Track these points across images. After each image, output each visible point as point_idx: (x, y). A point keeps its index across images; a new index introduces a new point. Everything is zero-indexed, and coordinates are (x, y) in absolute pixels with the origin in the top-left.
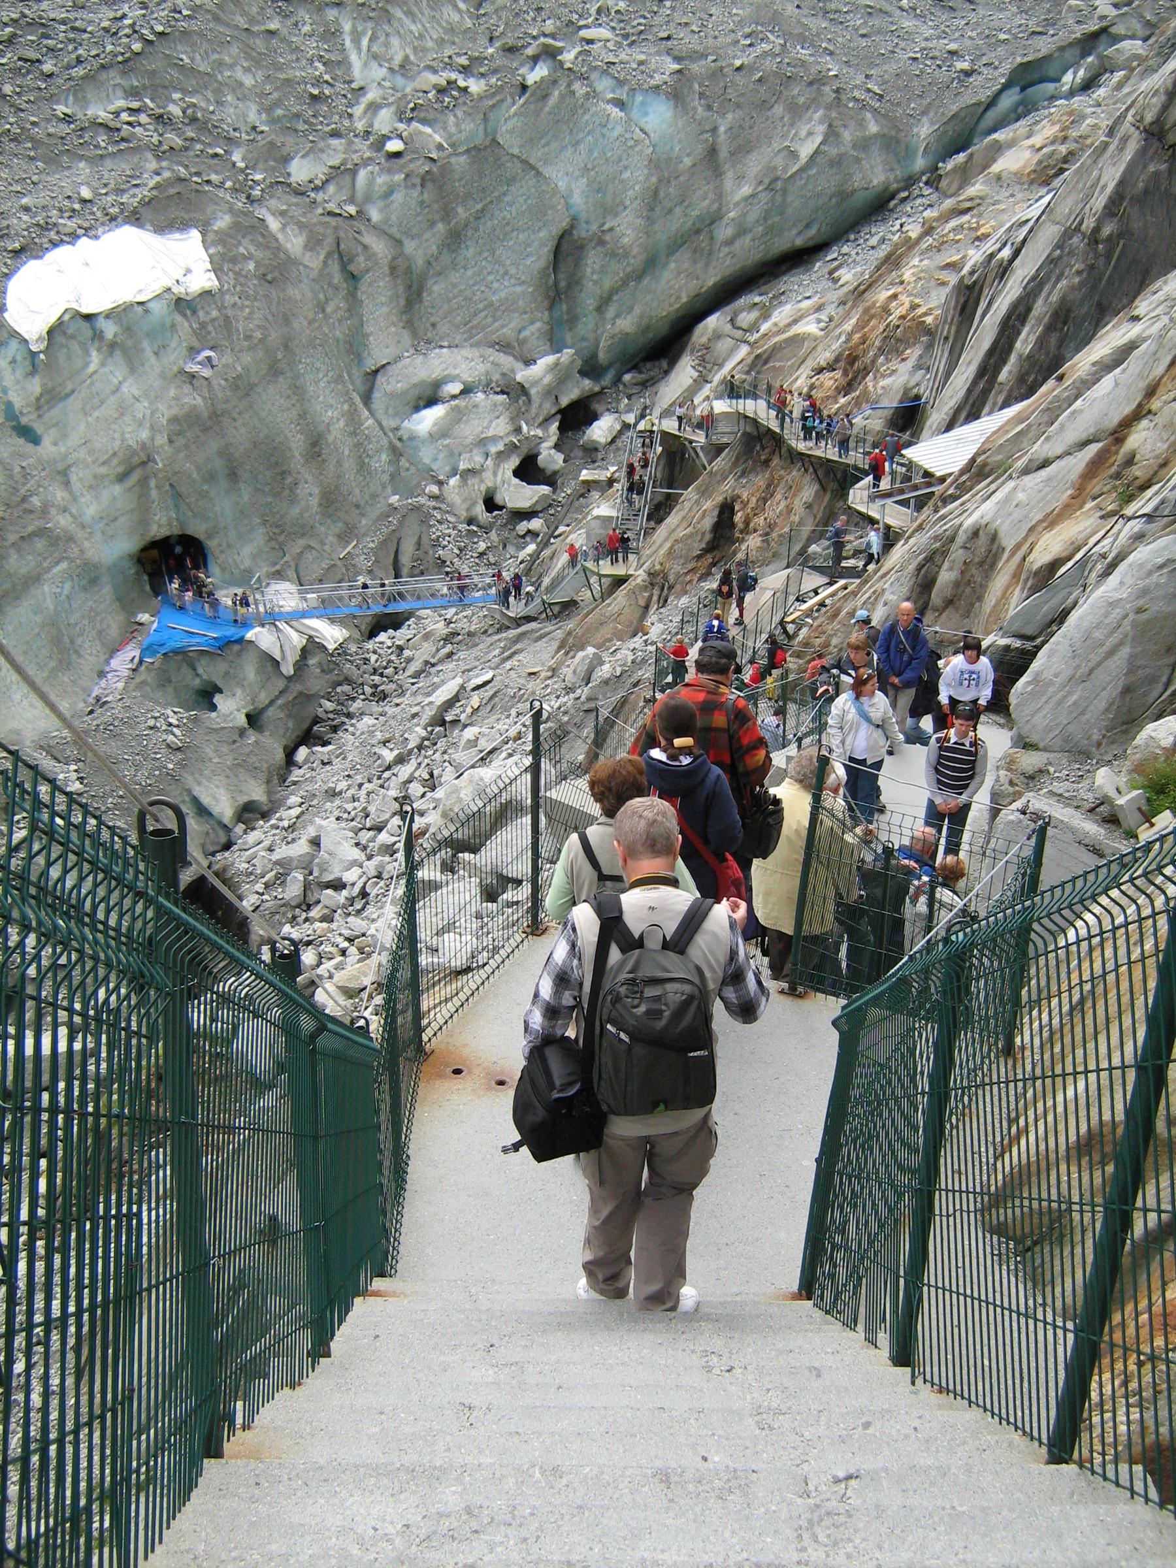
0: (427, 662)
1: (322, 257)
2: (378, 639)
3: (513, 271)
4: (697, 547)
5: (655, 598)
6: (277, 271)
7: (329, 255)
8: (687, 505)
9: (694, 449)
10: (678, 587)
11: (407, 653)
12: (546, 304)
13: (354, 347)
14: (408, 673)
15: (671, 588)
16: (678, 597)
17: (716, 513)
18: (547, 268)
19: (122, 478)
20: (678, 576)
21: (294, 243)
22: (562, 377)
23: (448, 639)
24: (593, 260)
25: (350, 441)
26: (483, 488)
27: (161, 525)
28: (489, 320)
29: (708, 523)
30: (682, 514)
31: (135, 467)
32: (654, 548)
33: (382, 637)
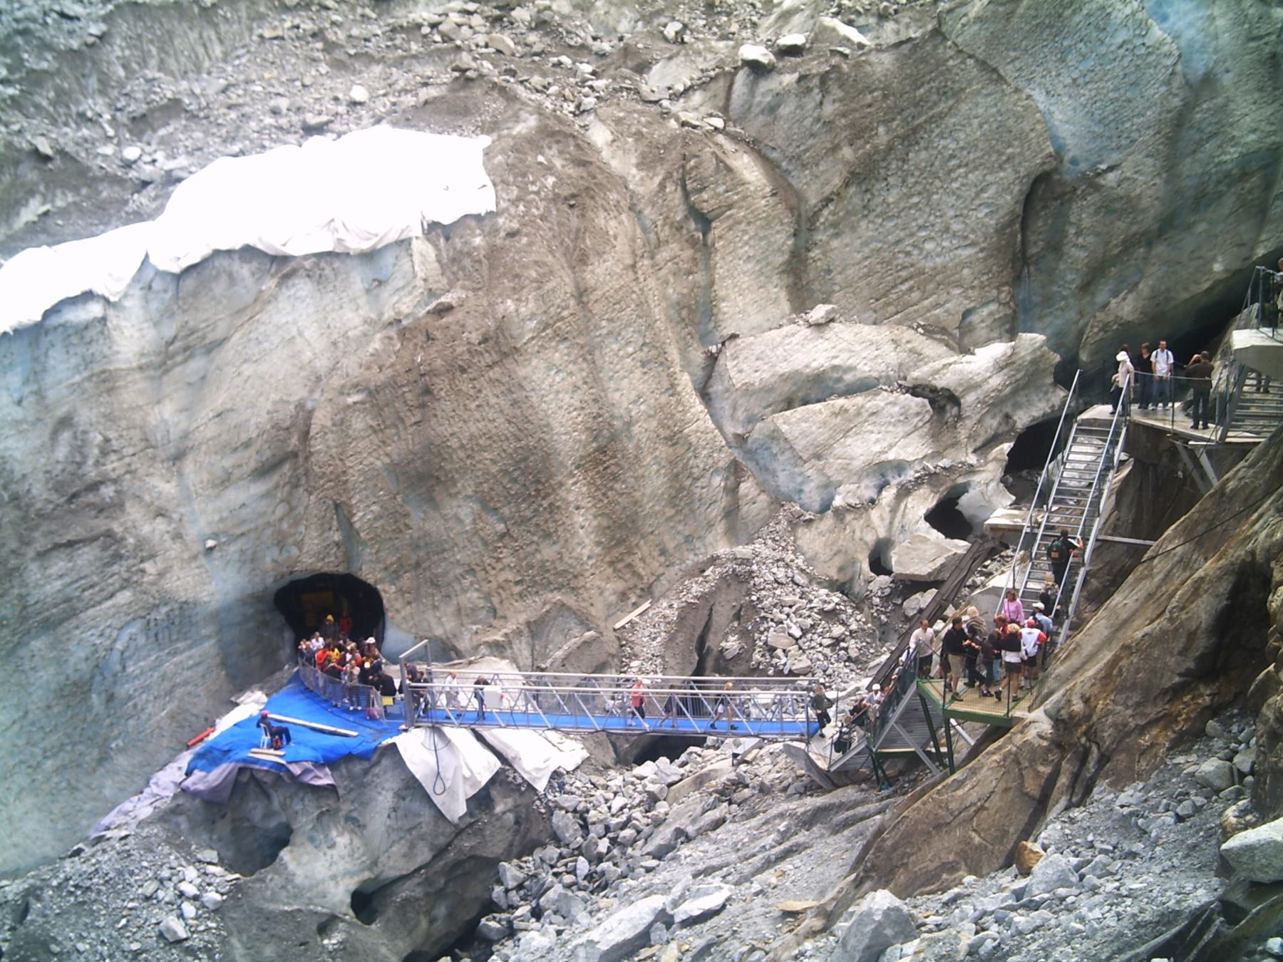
0: (679, 833)
1: (657, 180)
2: (638, 770)
3: (956, 226)
4: (1173, 667)
5: (1063, 780)
6: (584, 192)
7: (669, 176)
8: (1160, 567)
9: (1192, 452)
10: (1121, 759)
11: (662, 808)
12: (1007, 275)
13: (699, 314)
14: (651, 847)
15: (1104, 759)
16: (1118, 784)
17: (1224, 587)
18: (1010, 224)
19: (263, 471)
20: (1124, 733)
21: (621, 162)
22: (1024, 379)
23: (726, 793)
24: (1083, 214)
25: (663, 451)
26: (870, 538)
27: (313, 552)
28: (916, 295)
29: (1203, 611)
30: (1148, 585)
31: (286, 455)
32: (1075, 661)
33: (647, 768)
